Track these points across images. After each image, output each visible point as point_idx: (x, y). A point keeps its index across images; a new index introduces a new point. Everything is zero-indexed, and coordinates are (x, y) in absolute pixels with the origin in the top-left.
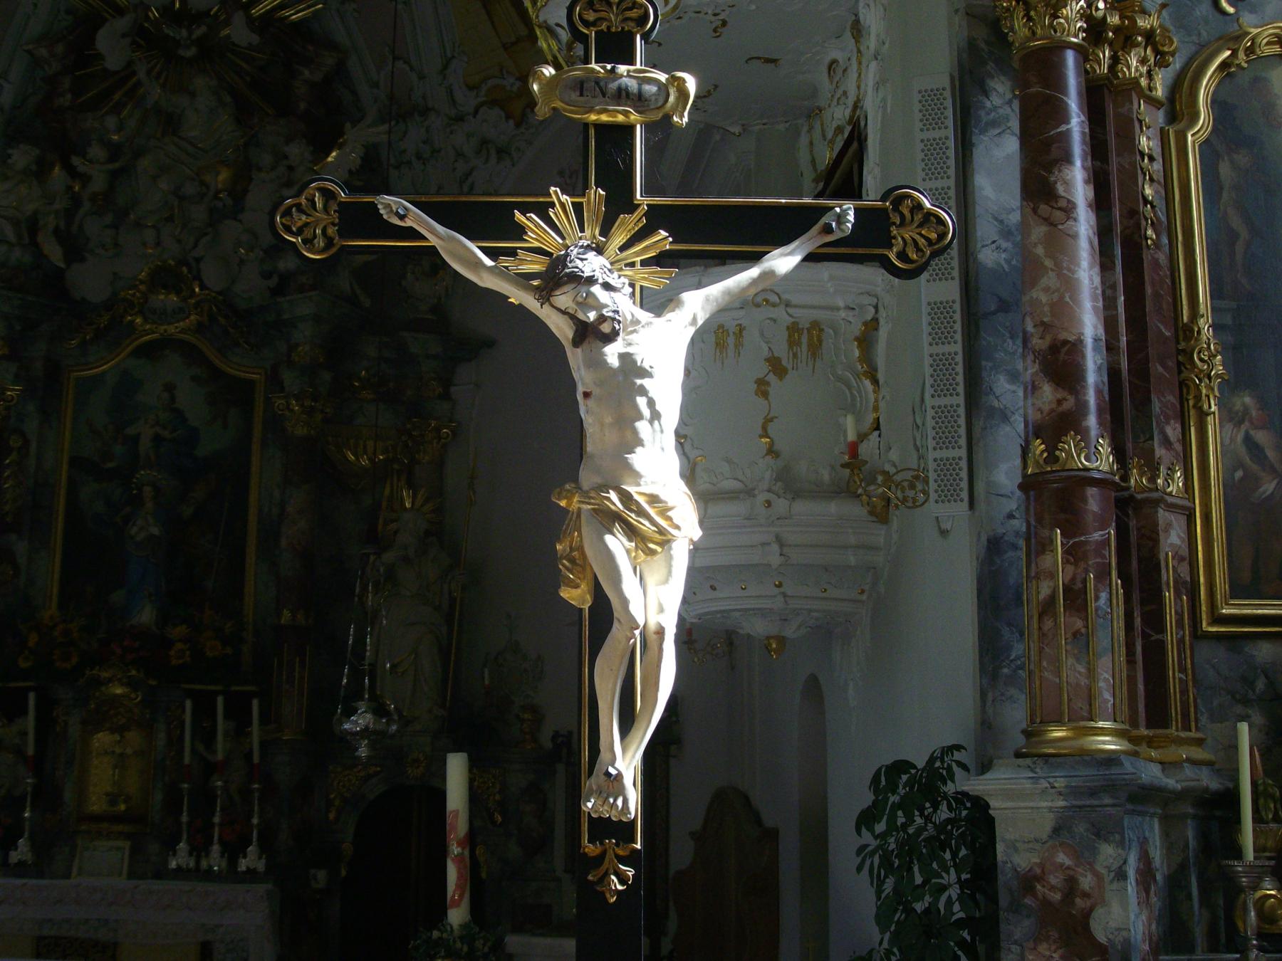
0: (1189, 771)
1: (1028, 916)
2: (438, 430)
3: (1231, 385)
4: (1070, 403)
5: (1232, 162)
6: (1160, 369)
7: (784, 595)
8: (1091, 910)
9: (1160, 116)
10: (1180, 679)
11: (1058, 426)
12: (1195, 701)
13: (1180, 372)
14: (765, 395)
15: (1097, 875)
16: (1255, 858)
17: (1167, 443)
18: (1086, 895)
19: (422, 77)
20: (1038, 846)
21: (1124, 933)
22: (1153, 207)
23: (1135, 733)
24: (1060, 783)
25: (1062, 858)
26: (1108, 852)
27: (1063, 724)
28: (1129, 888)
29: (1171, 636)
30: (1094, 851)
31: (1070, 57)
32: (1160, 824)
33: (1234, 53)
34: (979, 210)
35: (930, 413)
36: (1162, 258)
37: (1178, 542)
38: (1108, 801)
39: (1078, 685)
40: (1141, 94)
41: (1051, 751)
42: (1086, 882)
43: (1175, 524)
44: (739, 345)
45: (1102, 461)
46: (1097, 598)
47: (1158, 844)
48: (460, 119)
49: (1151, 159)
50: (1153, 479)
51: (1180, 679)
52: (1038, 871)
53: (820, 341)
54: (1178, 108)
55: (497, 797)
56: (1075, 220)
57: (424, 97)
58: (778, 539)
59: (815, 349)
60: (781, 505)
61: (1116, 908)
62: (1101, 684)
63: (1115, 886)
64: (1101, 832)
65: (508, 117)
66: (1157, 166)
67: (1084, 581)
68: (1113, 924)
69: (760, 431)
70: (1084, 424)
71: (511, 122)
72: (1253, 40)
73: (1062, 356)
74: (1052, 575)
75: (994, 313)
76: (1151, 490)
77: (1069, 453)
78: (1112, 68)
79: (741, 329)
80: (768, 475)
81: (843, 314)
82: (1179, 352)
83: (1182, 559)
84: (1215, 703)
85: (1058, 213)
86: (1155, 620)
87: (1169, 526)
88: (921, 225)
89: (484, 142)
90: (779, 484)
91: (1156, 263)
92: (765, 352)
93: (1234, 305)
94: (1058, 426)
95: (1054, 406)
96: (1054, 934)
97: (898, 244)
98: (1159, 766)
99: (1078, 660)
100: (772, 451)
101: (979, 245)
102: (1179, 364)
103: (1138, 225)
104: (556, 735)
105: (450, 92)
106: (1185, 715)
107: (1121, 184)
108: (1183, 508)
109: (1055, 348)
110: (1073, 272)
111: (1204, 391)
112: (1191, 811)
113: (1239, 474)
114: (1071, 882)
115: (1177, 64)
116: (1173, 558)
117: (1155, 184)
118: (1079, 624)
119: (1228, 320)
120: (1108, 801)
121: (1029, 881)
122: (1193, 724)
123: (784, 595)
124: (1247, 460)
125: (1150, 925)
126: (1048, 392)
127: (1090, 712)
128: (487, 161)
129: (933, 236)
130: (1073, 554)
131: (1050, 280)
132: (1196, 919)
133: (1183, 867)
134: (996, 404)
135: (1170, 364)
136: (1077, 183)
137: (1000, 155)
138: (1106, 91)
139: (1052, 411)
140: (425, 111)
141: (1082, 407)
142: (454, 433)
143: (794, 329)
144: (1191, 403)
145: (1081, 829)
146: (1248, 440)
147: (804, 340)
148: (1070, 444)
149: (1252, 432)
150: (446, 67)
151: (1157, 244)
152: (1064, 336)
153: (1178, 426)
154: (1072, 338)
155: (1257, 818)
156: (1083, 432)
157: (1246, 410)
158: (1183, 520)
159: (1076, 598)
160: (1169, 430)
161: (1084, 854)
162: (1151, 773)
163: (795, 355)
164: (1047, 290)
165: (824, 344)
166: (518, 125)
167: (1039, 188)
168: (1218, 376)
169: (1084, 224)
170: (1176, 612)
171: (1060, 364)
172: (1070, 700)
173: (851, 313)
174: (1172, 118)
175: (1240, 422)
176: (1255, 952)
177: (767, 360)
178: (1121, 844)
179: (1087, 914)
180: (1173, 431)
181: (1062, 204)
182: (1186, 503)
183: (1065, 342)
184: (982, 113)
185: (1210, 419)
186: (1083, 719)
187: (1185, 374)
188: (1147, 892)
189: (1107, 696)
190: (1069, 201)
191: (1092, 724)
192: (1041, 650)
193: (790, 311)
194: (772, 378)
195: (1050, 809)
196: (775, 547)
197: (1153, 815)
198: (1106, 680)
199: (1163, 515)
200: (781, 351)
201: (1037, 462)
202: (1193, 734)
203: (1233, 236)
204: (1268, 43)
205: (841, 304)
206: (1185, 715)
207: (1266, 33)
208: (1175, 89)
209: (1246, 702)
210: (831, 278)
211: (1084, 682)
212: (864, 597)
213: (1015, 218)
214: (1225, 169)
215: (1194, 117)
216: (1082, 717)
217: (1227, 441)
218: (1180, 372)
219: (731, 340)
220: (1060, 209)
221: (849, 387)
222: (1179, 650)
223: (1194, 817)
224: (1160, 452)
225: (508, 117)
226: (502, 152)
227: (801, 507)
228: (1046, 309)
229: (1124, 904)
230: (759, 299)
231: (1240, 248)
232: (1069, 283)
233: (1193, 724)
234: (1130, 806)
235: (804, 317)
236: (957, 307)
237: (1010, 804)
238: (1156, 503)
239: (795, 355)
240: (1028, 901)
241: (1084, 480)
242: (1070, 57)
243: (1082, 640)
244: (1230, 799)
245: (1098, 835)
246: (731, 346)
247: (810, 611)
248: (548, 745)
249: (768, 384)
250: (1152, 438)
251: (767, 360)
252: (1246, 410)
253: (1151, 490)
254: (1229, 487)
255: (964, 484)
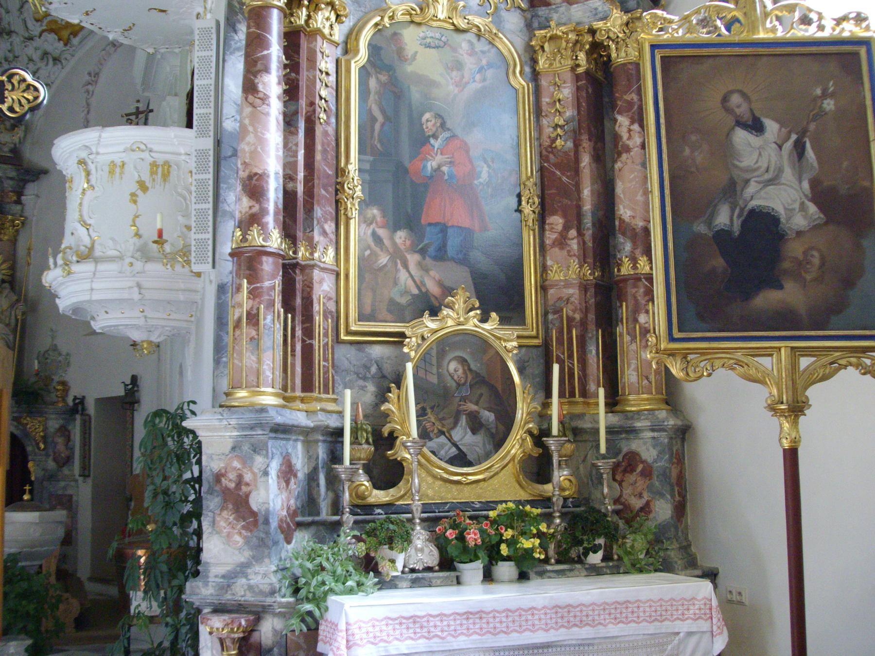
0: (321, 416)
1: (218, 496)
2: (13, 221)
3: (364, 204)
4: (256, 209)
5: (377, 78)
6: (323, 192)
7: (146, 317)
8: (250, 492)
9: (339, 51)
10: (324, 366)
11: (253, 220)
12: (333, 377)
13: (336, 194)
14: (135, 202)
15: (254, 474)
16: (351, 464)
17: (324, 233)
18: (247, 484)
19: (8, 12)
20: (223, 457)
21: (266, 505)
22: (326, 101)
23: (287, 394)
24: (233, 422)
25: (236, 464)
26: (259, 460)
27: (243, 389)
28: (270, 481)
29: (317, 343)
30: (252, 460)
31: (275, 13)
32: (303, 446)
33: (382, 18)
34: (225, 98)
35: (194, 213)
36: (331, 130)
37: (328, 289)
38: (260, 432)
39: (252, 367)
40: (324, 37)
41: (236, 404)
42: (248, 477)
43: (326, 279)
44: (122, 173)
45: (275, 241)
46: (265, 319)
47: (300, 456)
48: (31, 39)
49: (327, 74)
50: (312, 254)
51: (324, 366)
52: (223, 471)
53: (169, 172)
54: (348, 47)
55: (42, 434)
56: (268, 105)
57: (9, 24)
58: (139, 286)
59: (166, 177)
60: (139, 265)
61: (262, 492)
62: (265, 367)
63: (263, 479)
64: (257, 449)
65: (60, 39)
66: (332, 79)
67: (258, 309)
68: (261, 500)
69: (132, 223)
70: (264, 220)
71: (62, 42)
72: (393, 12)
73: (254, 182)
74: (240, 305)
75: (230, 157)
76: (310, 259)
77: (253, 236)
78: (307, 22)
79: (124, 164)
80: (132, 248)
81: (183, 157)
82: (338, 183)
83: (330, 299)
84: (348, 379)
85: (258, 101)
86: (309, 332)
87: (321, 282)
88: (24, 91)
89: (46, 54)
90: (139, 253)
91: (326, 133)
92: (137, 178)
93: (371, 158)
94: (253, 220)
95: (247, 209)
96: (230, 506)
97: (9, 101)
98: (305, 414)
99: (252, 354)
100: (137, 235)
101: (224, 118)
102: (337, 191)
103: (314, 111)
104: (75, 398)
105: (25, 21)
106: (326, 386)
107: (307, 86)
108: (334, 271)
109: (250, 177)
110: (263, 134)
111: (349, 206)
112: (321, 438)
113: (367, 253)
114: (240, 477)
115: (348, 23)
116: (324, 298)
117: (329, 89)
118: (254, 333)
119: (367, 166)
120: (260, 432)
121: (218, 477)
122: (331, 390)
123: (146, 317)
124: (372, 244)
125: (289, 501)
126: (246, 202)
127: (258, 382)
128: (47, 64)
129: (31, 98)
130: (254, 294)
131: (250, 138)
132: (322, 497)
133: (315, 470)
134: (227, 208)
135: (330, 189)
136: (272, 84)
137: (236, 66)
138: (302, 35)
139: (246, 212)
140: (10, 33)
141: (264, 212)
142: (23, 223)
143: (154, 165)
144: (342, 212)
145: (246, 448)
146: (374, 234)
147: (160, 170)
148: (255, 231)
149: (377, 230)
150: (22, 7)
151: (327, 122)
152: (256, 170)
153: (333, 225)
154: (260, 172)
155: (355, 441)
156: (263, 227)
157: (374, 217)
158: (333, 277)
159: (253, 318)
160: (326, 227)
161: (246, 461)
162: (300, 418)
163: (154, 180)
164: (248, 144)
165: (171, 175)
166: (66, 45)
167: (250, 87)
168: (357, 197)
169: (275, 108)
170: (324, 328)
171: (254, 188)
172: (247, 376)
173: (188, 157)
174: (346, 52)
175: (371, 223)
176: (348, 515)
177: (138, 182)
178: (267, 456)
179: (247, 496)
180: (330, 227)
181: (261, 95)
182: (335, 268)
183: (256, 174)
184: (232, 43)
185: (352, 222)
186: (253, 386)
187: (340, 195)
188: (287, 482)
189: (269, 373)
190: (265, 94)
191: (258, 389)
192: (234, 347)
193: (152, 154)
194: (139, 193)
195: (230, 437)
196: (136, 289)
197: (296, 440)
198: (268, 365)
199: (316, 274)
200: (146, 177)
201: (237, 242)
202: (330, 396)
203: (374, 120)
204: (402, 14)
205: (183, 152)
206: (326, 386)
207: (401, 9)
208: (348, 36)
209: (364, 378)
210: (176, 136)
211: (255, 365)
212: (193, 319)
213: (239, 102)
214: (373, 83)
215: (357, 51)
216: (255, 385)
217: (362, 234)
218: (336, 194)
219: (118, 170)
220: (259, 98)
221: (185, 199)
222: (324, 350)
223: (324, 441)
224: (317, 236)
225: (60, 39)
226: (56, 60)
227: (150, 266)
228: (247, 155)
229: (267, 489)
230: (134, 147)
231: (377, 126)
232: (261, 141)
233: (331, 390)
234: (273, 435)
235: (160, 158)
236: (211, 153)
237: (211, 434)
238: (313, 267)
239: (154, 180)
240: (217, 488)
241: (262, 252)
242: (275, 13)
243: (255, 341)
244: (339, 433)
245: (255, 451)
246: (118, 174)
247: (163, 327)
248: (71, 403)
249: (137, 196)
250: (313, 230)
251: (138, 182)
252: (374, 217)
253: (310, 259)
254: (361, 259)
255: (210, 254)
